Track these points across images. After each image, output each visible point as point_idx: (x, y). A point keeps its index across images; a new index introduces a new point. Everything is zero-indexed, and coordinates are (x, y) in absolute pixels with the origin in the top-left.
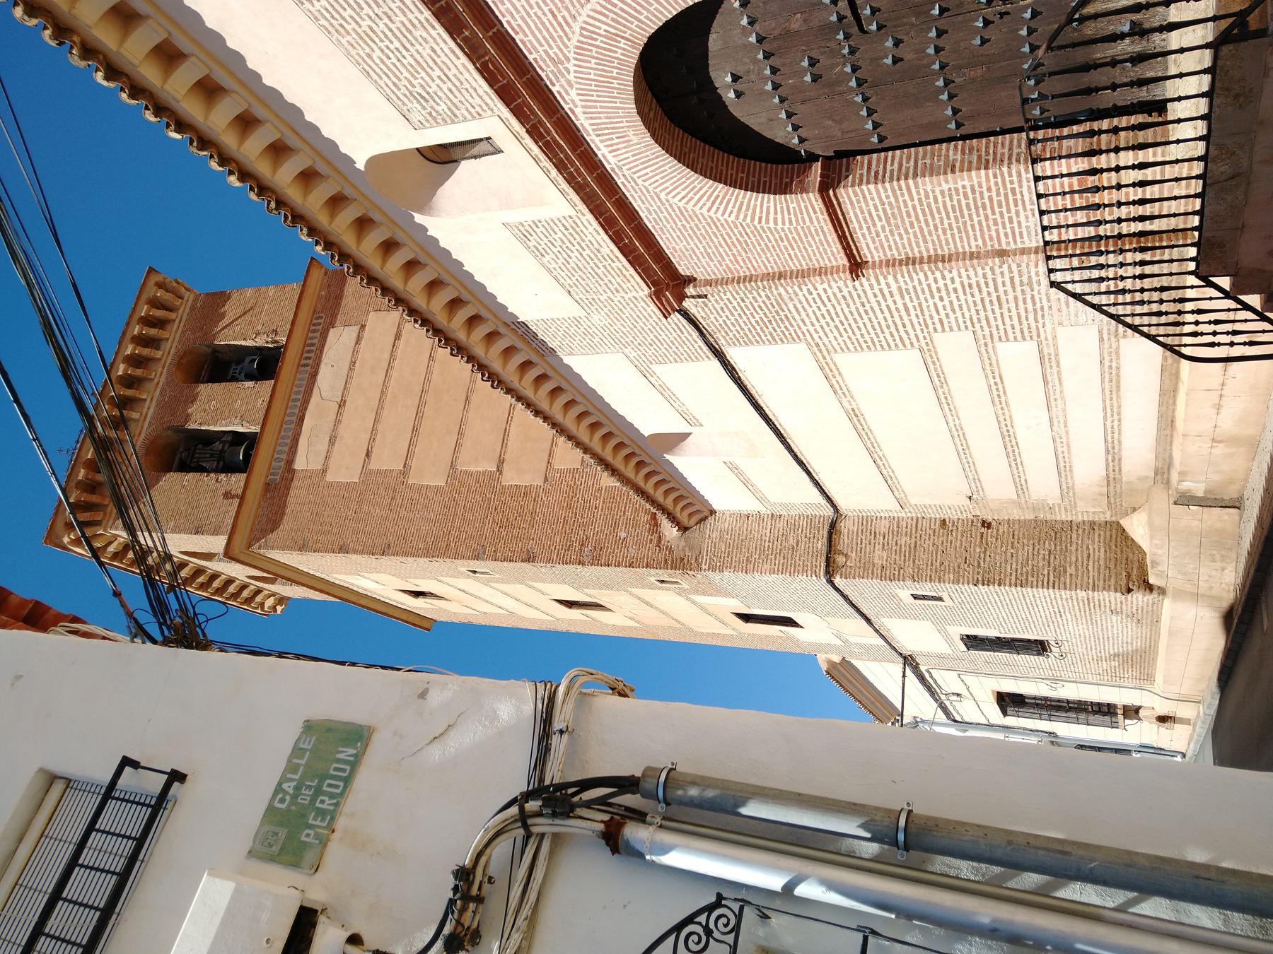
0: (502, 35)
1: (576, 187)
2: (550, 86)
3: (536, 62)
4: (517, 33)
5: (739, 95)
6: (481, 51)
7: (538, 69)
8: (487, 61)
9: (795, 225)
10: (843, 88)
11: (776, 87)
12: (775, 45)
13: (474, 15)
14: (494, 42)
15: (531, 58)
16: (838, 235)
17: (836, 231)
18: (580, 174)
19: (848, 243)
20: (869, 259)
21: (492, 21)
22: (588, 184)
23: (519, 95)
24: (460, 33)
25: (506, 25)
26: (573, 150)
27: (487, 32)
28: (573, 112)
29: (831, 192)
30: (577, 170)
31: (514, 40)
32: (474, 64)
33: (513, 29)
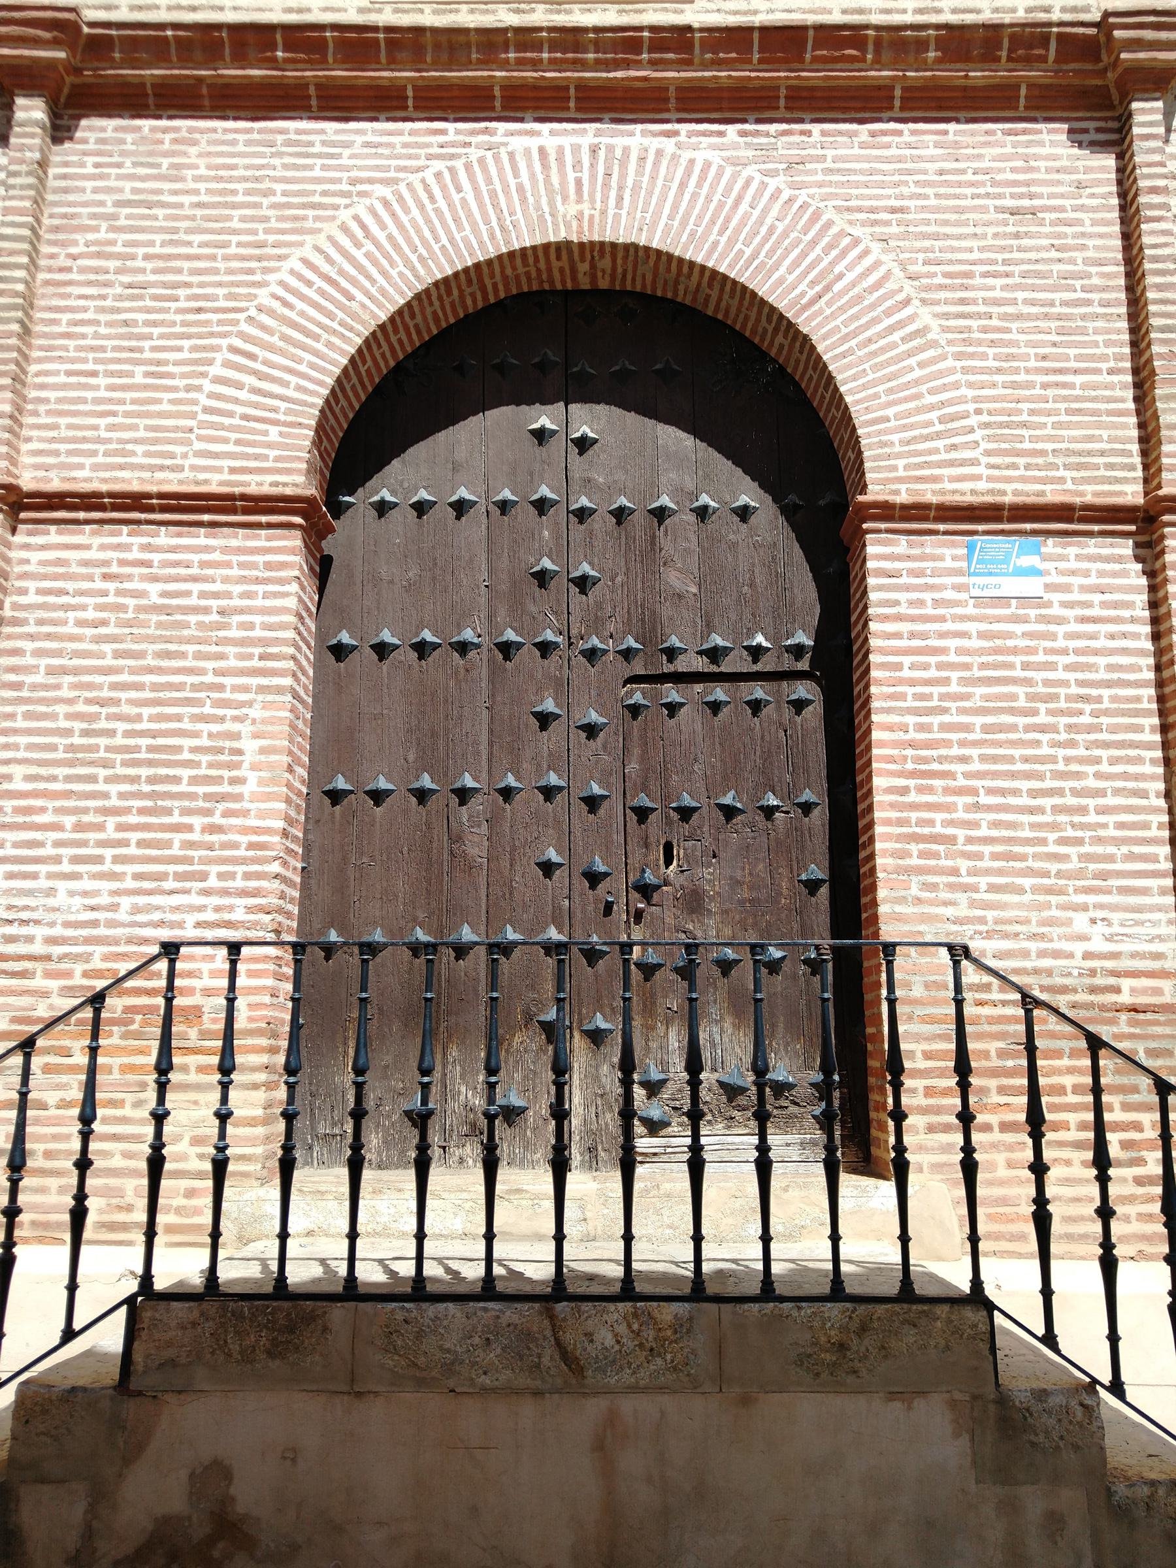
0: (880, 109)
1: (500, 39)
2: (739, 126)
3: (802, 133)
4: (873, 134)
5: (541, 435)
6: (886, 56)
7: (785, 126)
8: (864, 51)
9: (202, 417)
10: (502, 616)
11: (541, 506)
12: (639, 533)
13: (476, 88)
14: (879, 88)
15: (816, 128)
16: (149, 496)
17: (161, 496)
18: (521, 63)
19: (102, 508)
20: (19, 539)
21: (912, 109)
22: (484, 64)
23: (767, 62)
24: (940, 43)
25: (892, 126)
26: (582, 86)
27: (904, 89)
28: (668, 134)
29: (298, 520)
30: (536, 64)
31: (862, 121)
32: (878, 28)
33: (884, 133)
